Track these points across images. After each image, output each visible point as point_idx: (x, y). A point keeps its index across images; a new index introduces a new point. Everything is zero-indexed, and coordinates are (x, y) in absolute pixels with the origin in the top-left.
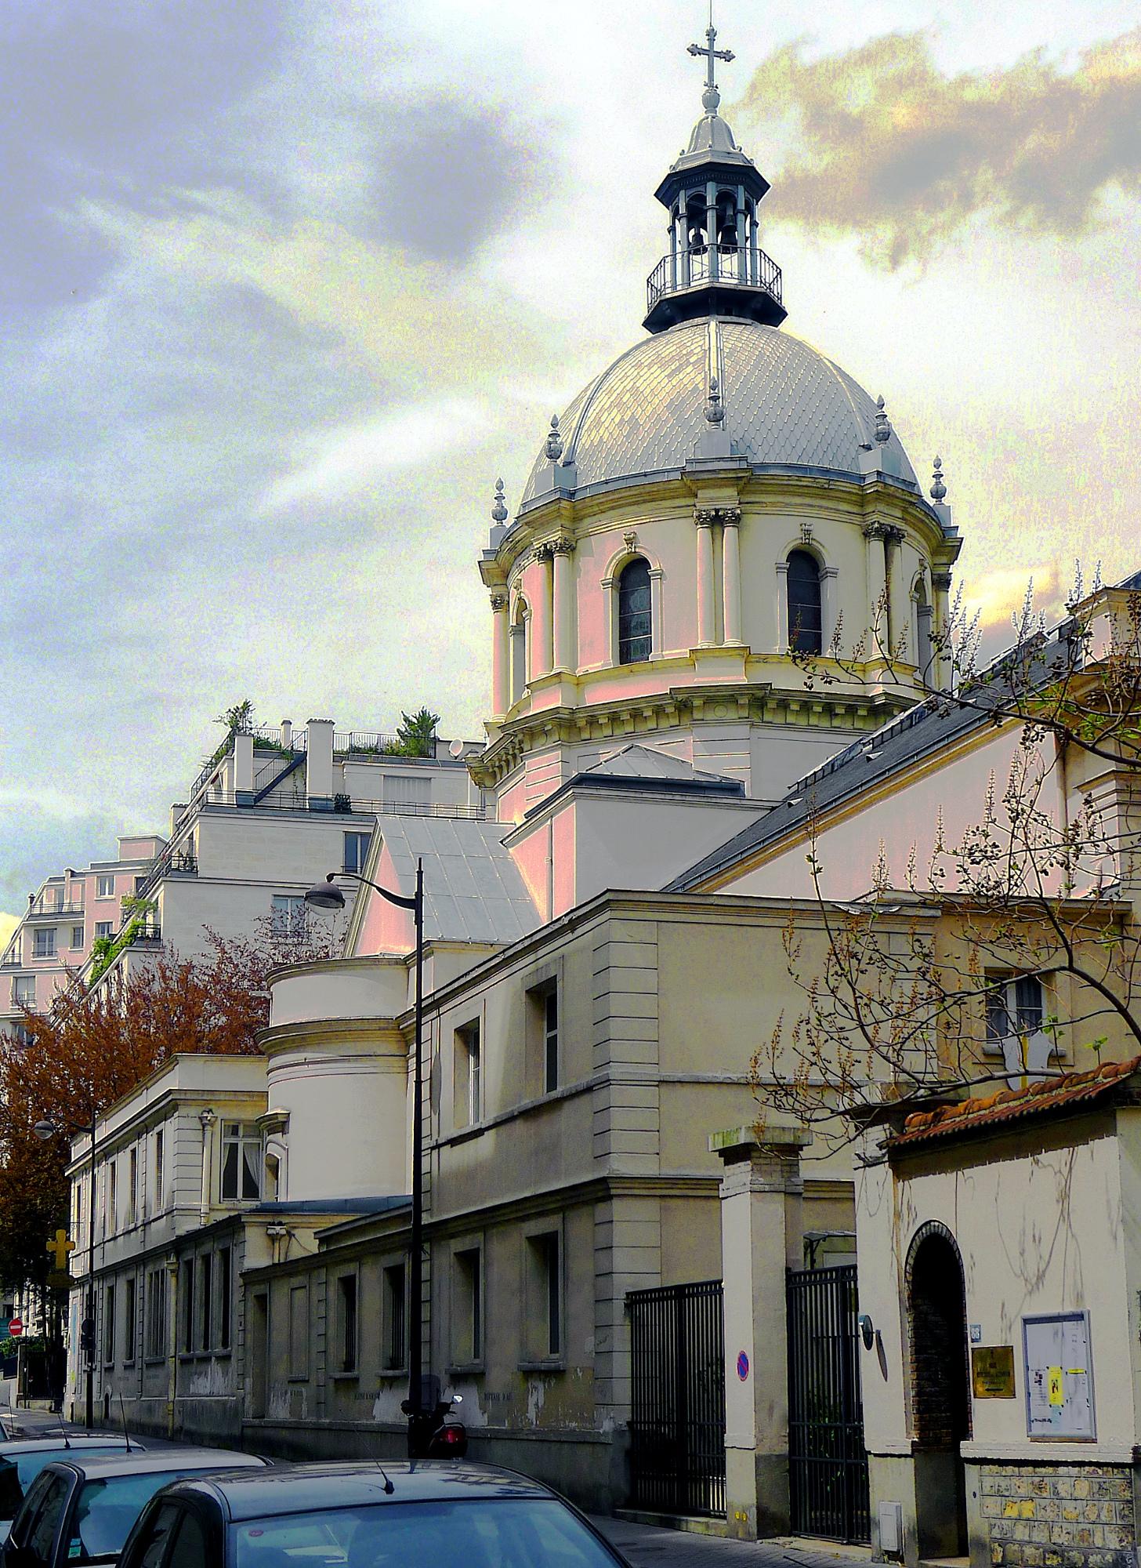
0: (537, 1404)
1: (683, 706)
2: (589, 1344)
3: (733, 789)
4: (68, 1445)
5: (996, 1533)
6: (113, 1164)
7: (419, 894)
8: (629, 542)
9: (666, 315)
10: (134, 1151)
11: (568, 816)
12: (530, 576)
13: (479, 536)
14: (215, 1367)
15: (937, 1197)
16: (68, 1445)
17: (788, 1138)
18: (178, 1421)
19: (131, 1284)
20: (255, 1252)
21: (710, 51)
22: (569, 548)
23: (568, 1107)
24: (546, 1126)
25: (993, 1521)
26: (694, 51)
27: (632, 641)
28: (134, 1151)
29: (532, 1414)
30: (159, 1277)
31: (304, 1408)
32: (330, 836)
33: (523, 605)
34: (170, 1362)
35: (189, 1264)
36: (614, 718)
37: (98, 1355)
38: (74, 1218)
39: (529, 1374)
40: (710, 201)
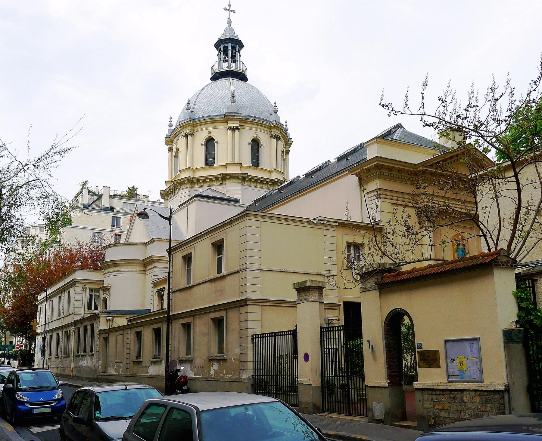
0: (214, 370)
1: (224, 178)
2: (238, 351)
3: (237, 201)
4: (126, 388)
5: (431, 414)
6: (53, 301)
7: (170, 216)
8: (209, 133)
9: (216, 77)
10: (60, 297)
11: (193, 207)
12: (181, 142)
13: (165, 131)
14: (88, 358)
15: (398, 301)
16: (126, 388)
17: (321, 285)
18: (74, 374)
19: (58, 335)
20: (102, 325)
21: (229, 10)
22: (192, 134)
23: (228, 278)
24: (218, 284)
25: (429, 410)
26: (225, 9)
27: (209, 161)
28: (60, 297)
29: (212, 372)
30: (68, 332)
31: (121, 370)
32: (108, 217)
33: (178, 150)
34: (72, 357)
35: (79, 329)
36: (204, 181)
37: (46, 354)
38: (38, 316)
39: (211, 360)
40: (230, 48)
